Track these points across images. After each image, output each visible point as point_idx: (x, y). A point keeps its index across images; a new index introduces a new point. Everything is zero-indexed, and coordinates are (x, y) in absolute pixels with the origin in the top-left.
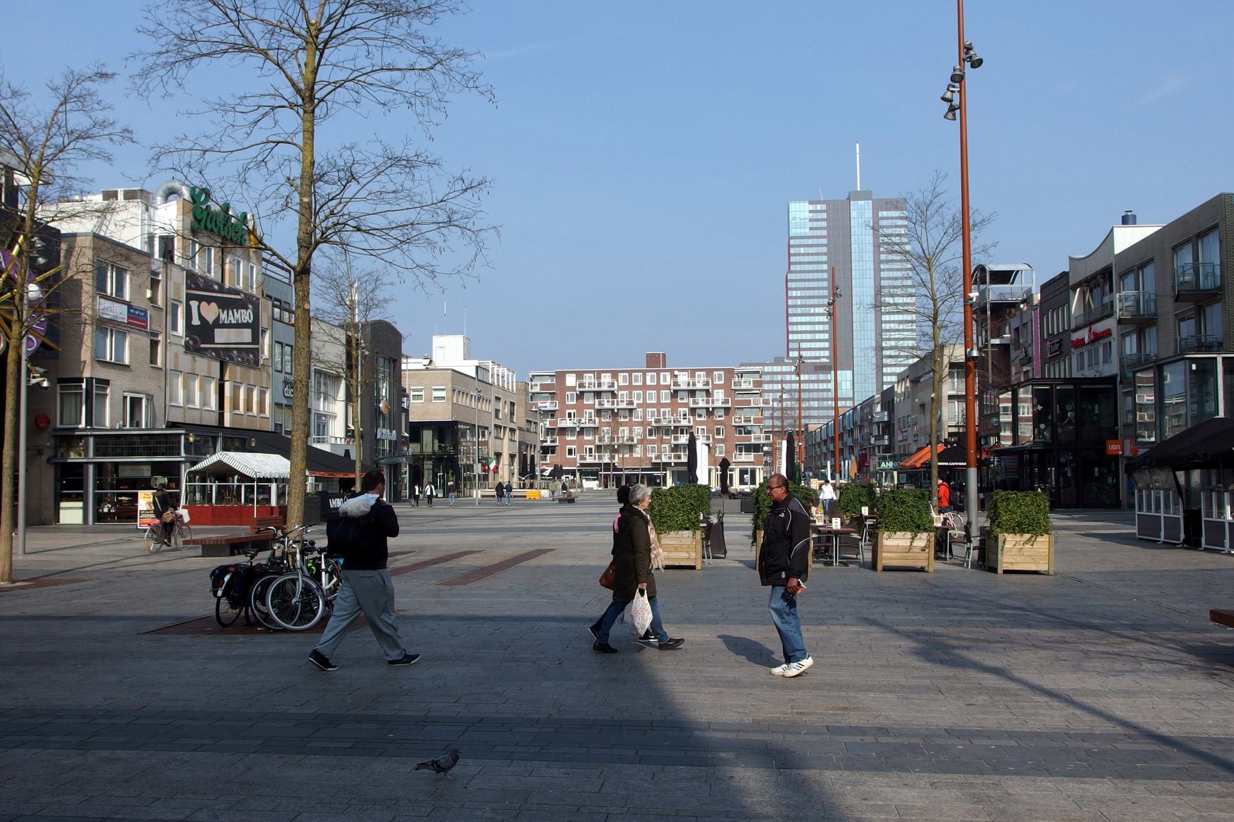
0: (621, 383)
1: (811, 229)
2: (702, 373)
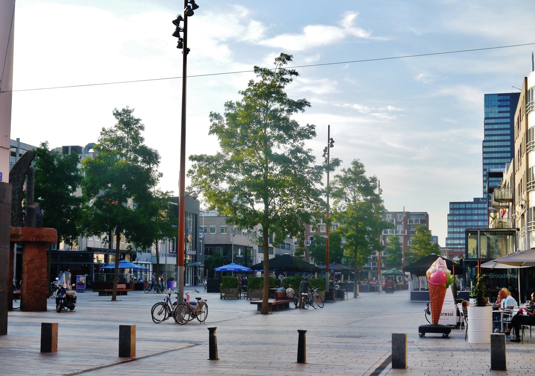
1: (499, 112)
2: (390, 215)
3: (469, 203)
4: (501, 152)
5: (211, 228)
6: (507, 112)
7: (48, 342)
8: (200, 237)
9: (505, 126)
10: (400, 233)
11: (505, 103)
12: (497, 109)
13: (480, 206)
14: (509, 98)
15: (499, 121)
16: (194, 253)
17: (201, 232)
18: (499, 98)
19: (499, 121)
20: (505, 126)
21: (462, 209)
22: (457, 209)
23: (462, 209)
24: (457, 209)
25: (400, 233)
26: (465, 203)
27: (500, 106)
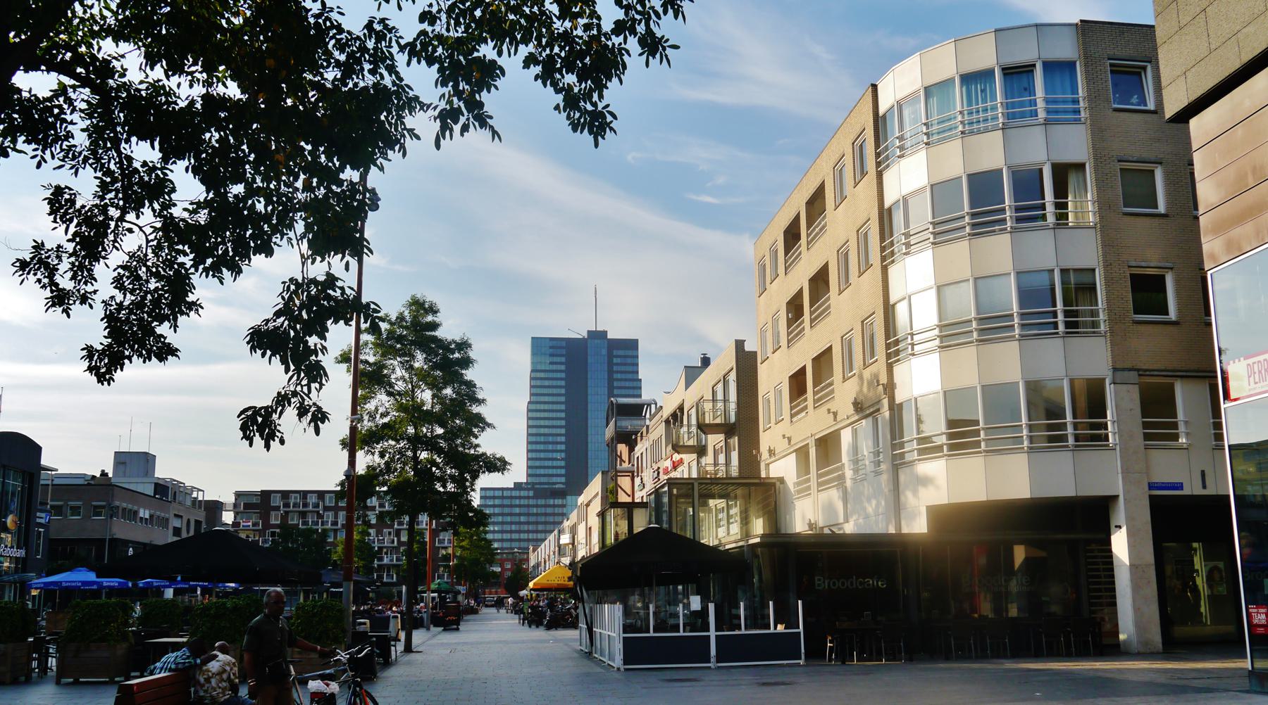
0: (327, 504)
3: (508, 489)
4: (553, 419)
5: (72, 508)
6: (561, 363)
7: (675, 47)
8: (38, 520)
9: (619, 376)
10: (311, 508)
11: (559, 351)
12: (548, 360)
13: (523, 493)
14: (564, 344)
15: (551, 375)
16: (21, 553)
17: (41, 511)
18: (551, 344)
19: (551, 375)
20: (619, 376)
21: (498, 498)
22: (490, 498)
23: (498, 498)
24: (490, 498)
25: (311, 508)
26: (503, 489)
27: (552, 355)
